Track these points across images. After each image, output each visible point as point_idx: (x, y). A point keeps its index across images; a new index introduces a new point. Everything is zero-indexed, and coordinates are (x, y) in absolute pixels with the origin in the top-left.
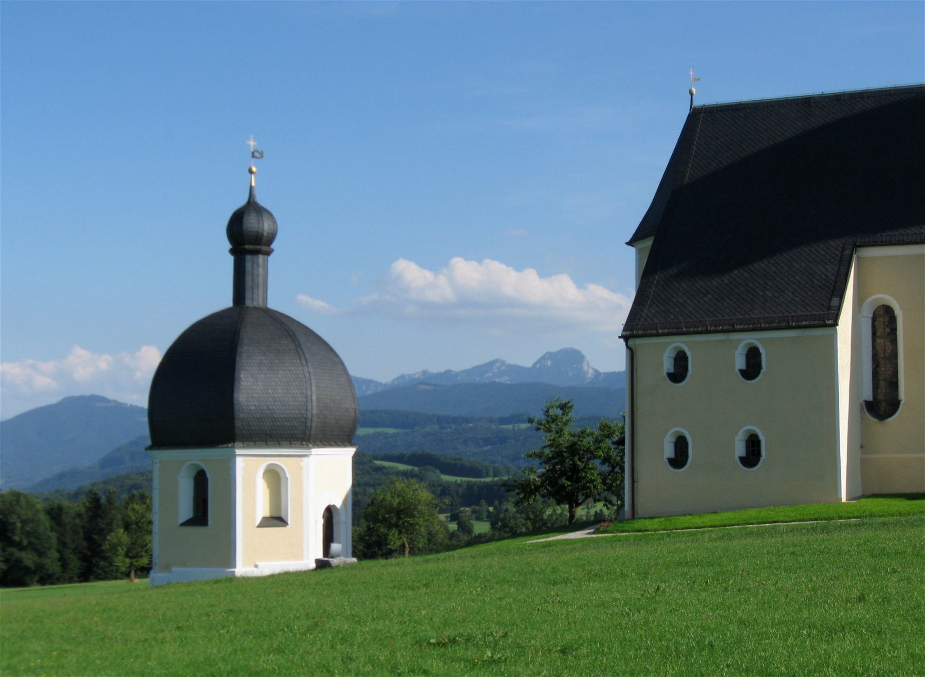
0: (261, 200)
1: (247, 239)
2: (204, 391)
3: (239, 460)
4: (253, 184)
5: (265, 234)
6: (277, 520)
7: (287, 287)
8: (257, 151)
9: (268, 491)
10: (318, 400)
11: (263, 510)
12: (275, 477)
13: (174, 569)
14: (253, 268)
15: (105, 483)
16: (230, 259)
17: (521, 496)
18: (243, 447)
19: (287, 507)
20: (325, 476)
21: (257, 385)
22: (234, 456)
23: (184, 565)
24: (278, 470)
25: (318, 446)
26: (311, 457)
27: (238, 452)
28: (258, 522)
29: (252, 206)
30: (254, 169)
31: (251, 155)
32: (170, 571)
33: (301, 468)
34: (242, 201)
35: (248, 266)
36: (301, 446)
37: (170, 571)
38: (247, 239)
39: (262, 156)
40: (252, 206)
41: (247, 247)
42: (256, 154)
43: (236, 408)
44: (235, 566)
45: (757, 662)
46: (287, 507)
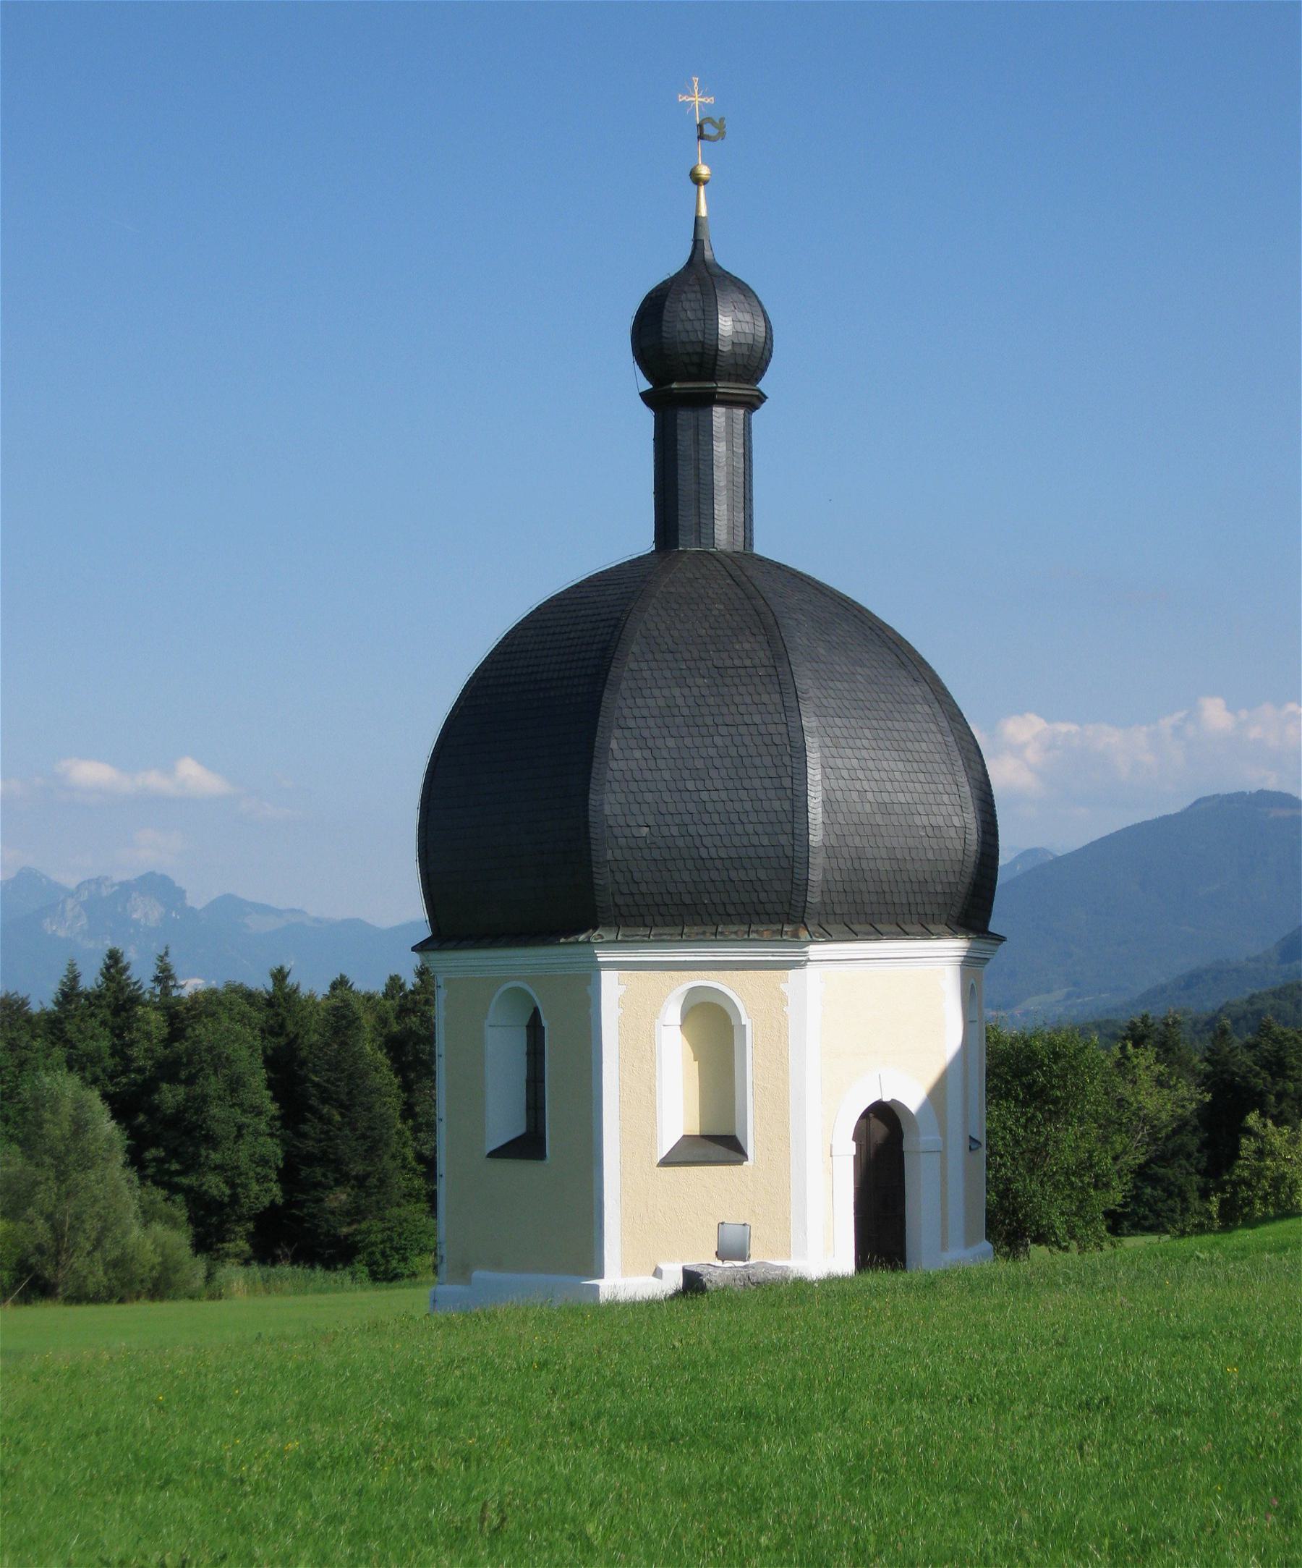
0: (723, 254)
1: (690, 366)
2: (587, 780)
3: (609, 980)
4: (703, 213)
5: (725, 347)
6: (719, 1144)
7: (802, 495)
8: (709, 120)
9: (695, 1065)
10: (828, 804)
11: (678, 1116)
12: (714, 1028)
13: (478, 1274)
14: (697, 442)
15: (1277, 994)
16: (646, 418)
17: (308, 1115)
18: (615, 943)
19: (759, 1100)
20: (874, 1023)
21: (642, 778)
22: (598, 967)
23: (497, 1265)
24: (709, 999)
25: (829, 938)
26: (810, 970)
27: (603, 956)
28: (667, 1142)
29: (701, 278)
30: (704, 171)
31: (696, 133)
32: (468, 1281)
33: (783, 999)
34: (676, 261)
35: (685, 438)
36: (778, 938)
37: (468, 1281)
38: (690, 366)
39: (722, 135)
40: (701, 278)
41: (674, 386)
42: (708, 130)
43: (594, 832)
44: (600, 1275)
45: (789, 1489)
46: (759, 1100)
